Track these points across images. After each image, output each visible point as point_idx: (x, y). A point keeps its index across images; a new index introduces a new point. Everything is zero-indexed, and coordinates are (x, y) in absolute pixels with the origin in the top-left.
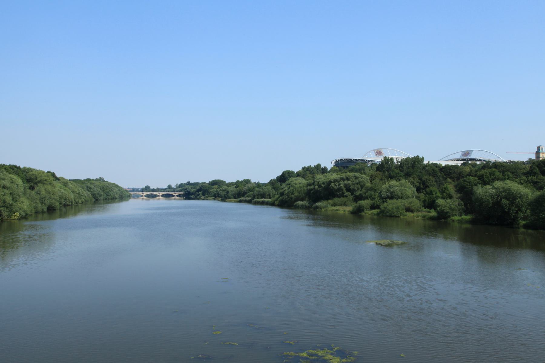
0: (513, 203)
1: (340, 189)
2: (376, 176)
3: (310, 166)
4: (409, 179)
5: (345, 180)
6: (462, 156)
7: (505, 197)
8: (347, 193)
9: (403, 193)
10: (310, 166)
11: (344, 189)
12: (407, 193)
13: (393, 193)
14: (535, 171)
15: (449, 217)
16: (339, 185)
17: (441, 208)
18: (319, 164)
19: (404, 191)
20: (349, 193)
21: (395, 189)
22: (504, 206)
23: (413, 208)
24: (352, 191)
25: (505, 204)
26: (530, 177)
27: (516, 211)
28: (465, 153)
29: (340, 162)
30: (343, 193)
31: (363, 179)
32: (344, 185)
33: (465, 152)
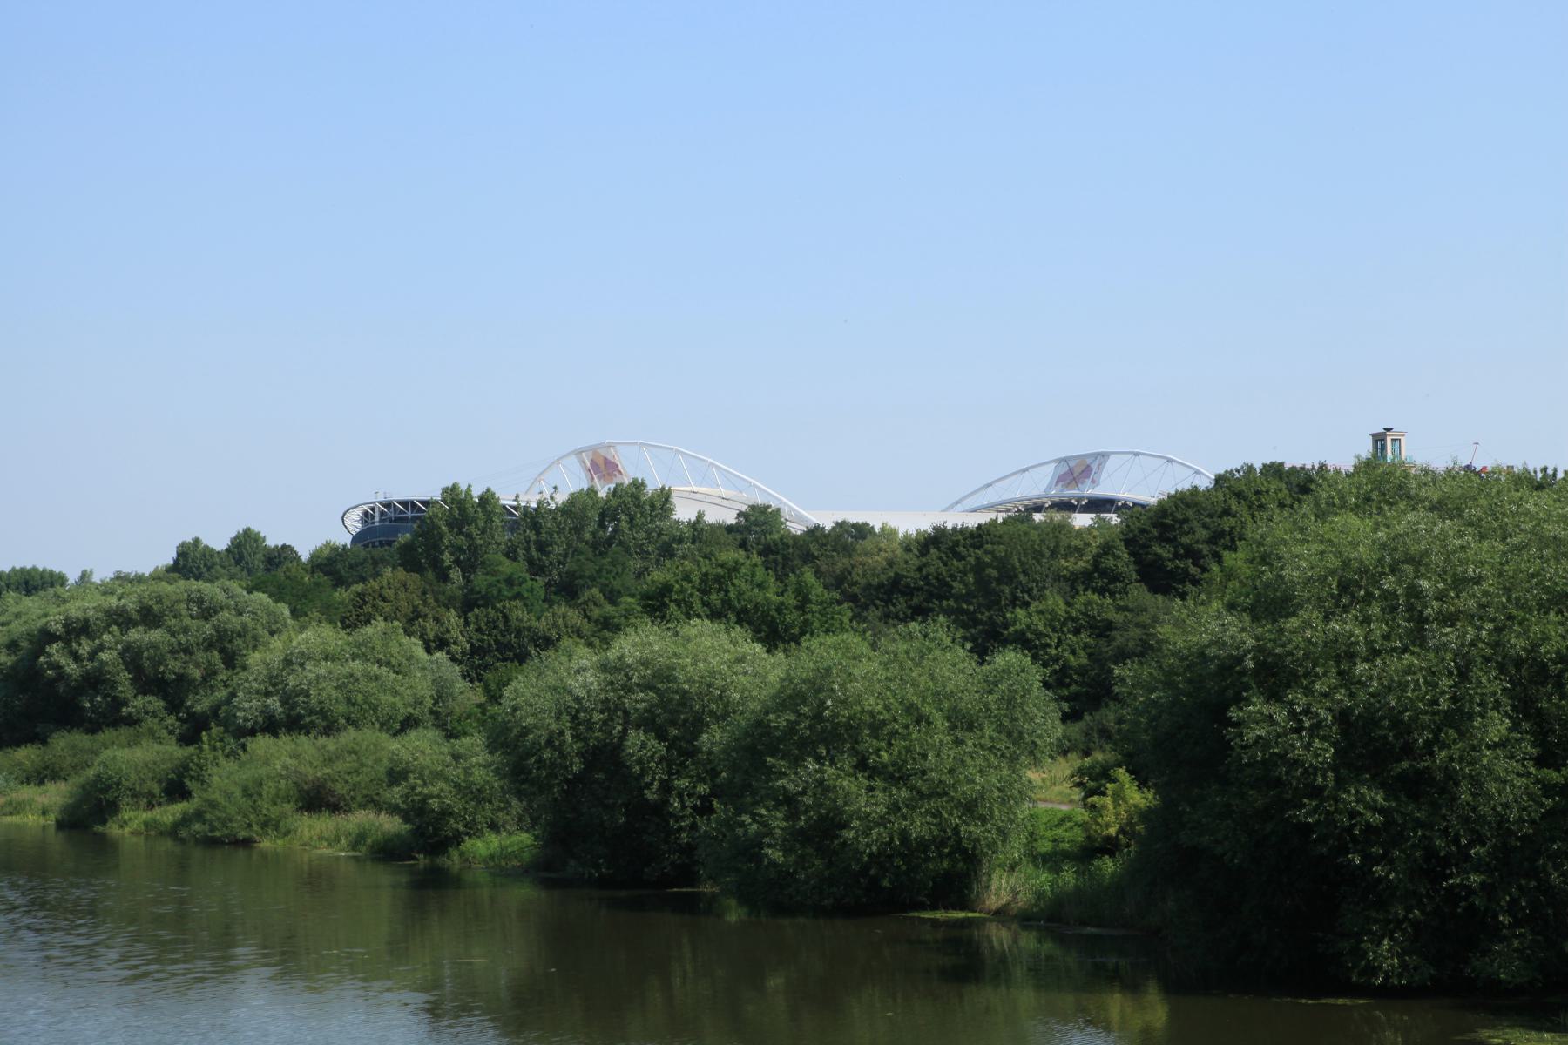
0: (692, 753)
1: (95, 681)
2: (384, 600)
3: (197, 541)
4: (554, 615)
5: (135, 624)
6: (1058, 482)
7: (648, 722)
8: (140, 701)
9: (360, 697)
10: (197, 541)
11: (125, 677)
12: (386, 698)
13: (302, 699)
14: (1111, 562)
15: (457, 839)
16: (93, 655)
17: (413, 788)
18: (247, 532)
19: (363, 684)
20: (156, 703)
21: (311, 671)
22: (637, 769)
23: (340, 789)
24: (172, 691)
25: (640, 761)
26: (1081, 599)
27: (701, 797)
28: (1071, 471)
29: (381, 521)
30: (115, 699)
31: (246, 618)
32: (121, 655)
33: (1072, 464)
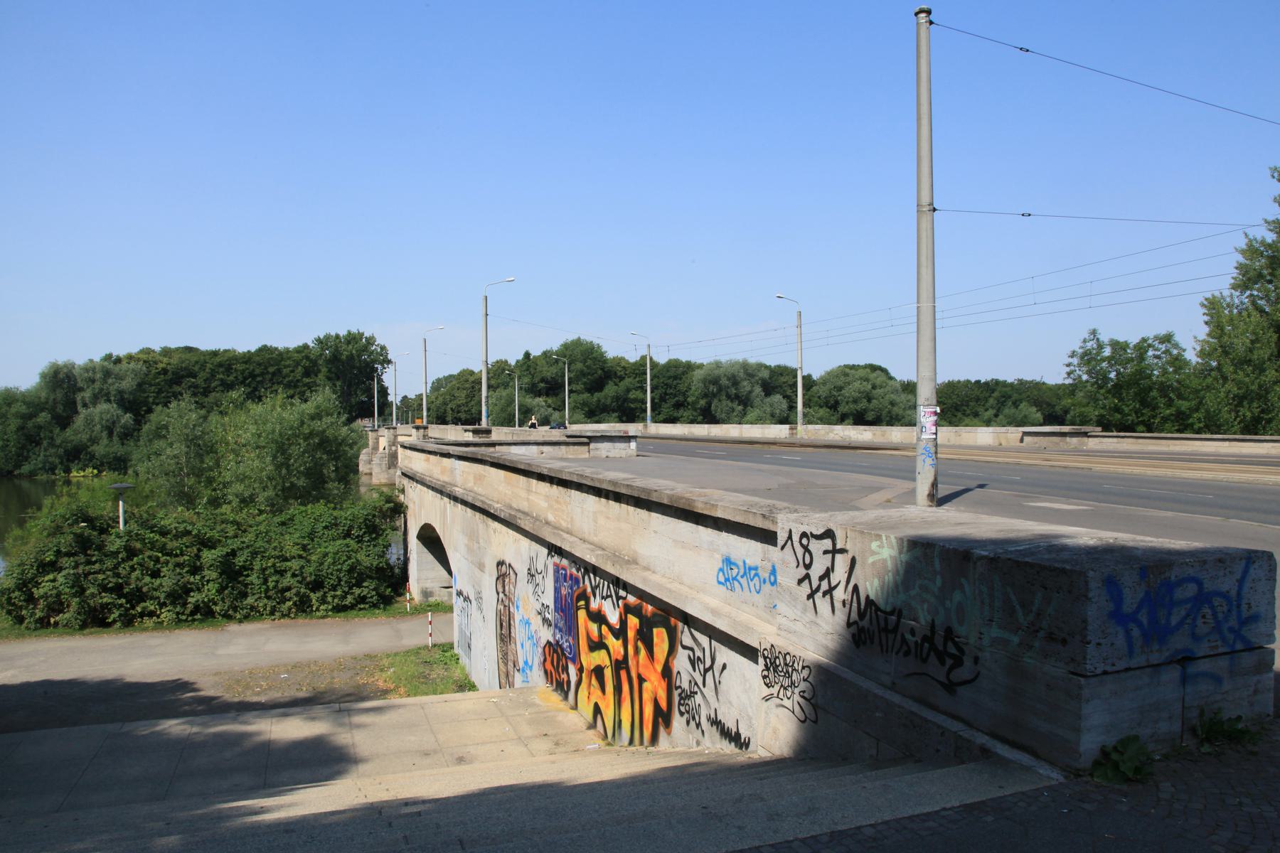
3: (579, 338)
10: (579, 338)
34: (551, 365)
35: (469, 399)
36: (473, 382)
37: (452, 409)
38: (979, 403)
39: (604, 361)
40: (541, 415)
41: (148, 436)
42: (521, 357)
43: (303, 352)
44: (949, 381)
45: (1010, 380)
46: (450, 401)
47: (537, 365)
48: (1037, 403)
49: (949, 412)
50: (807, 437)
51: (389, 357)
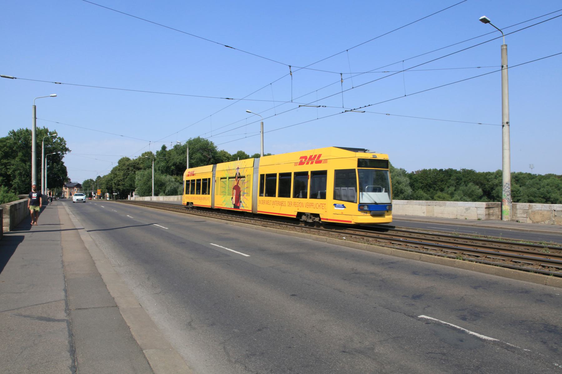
3: (199, 137)
10: (199, 137)
34: (180, 155)
35: (126, 177)
36: (128, 165)
37: (114, 183)
38: (443, 183)
39: (216, 153)
40: (171, 187)
41: (389, 350)
42: (160, 149)
43: (5, 142)
44: (424, 169)
45: (458, 170)
46: (114, 178)
47: (171, 155)
48: (481, 184)
49: (425, 188)
50: (529, 221)
51: (67, 146)
